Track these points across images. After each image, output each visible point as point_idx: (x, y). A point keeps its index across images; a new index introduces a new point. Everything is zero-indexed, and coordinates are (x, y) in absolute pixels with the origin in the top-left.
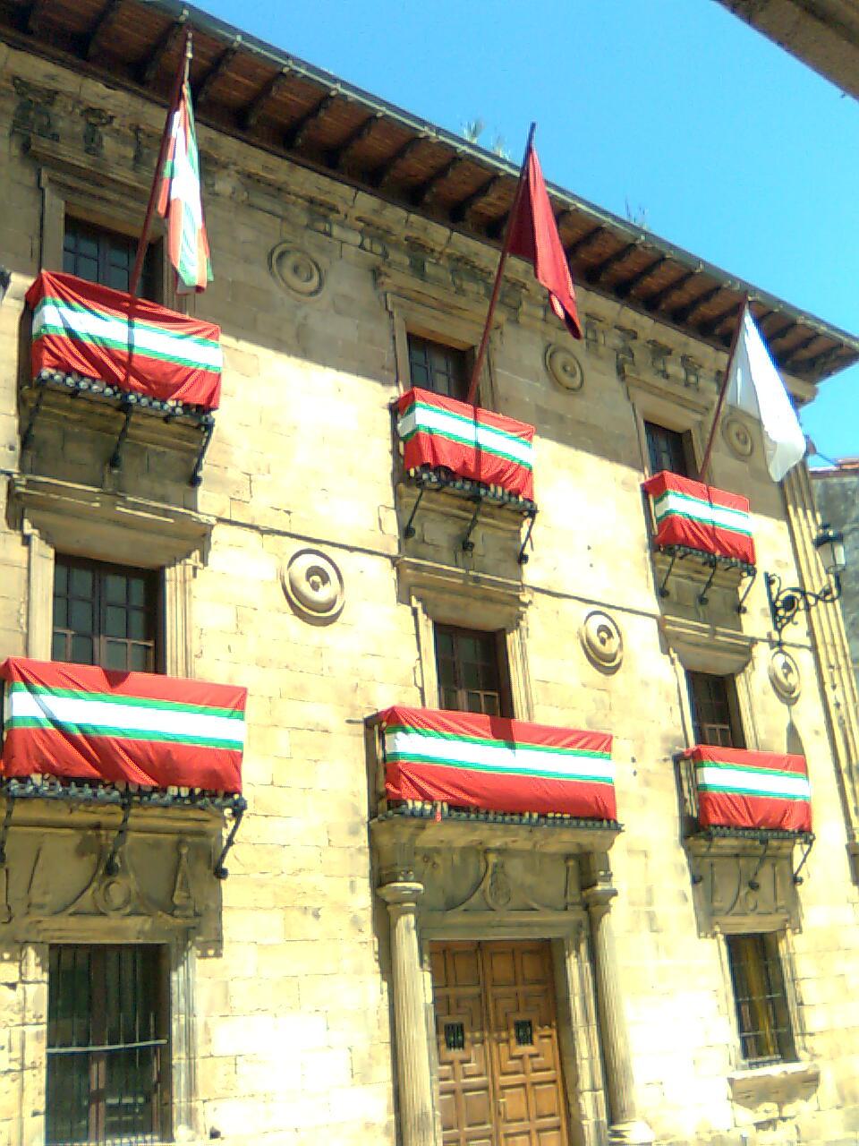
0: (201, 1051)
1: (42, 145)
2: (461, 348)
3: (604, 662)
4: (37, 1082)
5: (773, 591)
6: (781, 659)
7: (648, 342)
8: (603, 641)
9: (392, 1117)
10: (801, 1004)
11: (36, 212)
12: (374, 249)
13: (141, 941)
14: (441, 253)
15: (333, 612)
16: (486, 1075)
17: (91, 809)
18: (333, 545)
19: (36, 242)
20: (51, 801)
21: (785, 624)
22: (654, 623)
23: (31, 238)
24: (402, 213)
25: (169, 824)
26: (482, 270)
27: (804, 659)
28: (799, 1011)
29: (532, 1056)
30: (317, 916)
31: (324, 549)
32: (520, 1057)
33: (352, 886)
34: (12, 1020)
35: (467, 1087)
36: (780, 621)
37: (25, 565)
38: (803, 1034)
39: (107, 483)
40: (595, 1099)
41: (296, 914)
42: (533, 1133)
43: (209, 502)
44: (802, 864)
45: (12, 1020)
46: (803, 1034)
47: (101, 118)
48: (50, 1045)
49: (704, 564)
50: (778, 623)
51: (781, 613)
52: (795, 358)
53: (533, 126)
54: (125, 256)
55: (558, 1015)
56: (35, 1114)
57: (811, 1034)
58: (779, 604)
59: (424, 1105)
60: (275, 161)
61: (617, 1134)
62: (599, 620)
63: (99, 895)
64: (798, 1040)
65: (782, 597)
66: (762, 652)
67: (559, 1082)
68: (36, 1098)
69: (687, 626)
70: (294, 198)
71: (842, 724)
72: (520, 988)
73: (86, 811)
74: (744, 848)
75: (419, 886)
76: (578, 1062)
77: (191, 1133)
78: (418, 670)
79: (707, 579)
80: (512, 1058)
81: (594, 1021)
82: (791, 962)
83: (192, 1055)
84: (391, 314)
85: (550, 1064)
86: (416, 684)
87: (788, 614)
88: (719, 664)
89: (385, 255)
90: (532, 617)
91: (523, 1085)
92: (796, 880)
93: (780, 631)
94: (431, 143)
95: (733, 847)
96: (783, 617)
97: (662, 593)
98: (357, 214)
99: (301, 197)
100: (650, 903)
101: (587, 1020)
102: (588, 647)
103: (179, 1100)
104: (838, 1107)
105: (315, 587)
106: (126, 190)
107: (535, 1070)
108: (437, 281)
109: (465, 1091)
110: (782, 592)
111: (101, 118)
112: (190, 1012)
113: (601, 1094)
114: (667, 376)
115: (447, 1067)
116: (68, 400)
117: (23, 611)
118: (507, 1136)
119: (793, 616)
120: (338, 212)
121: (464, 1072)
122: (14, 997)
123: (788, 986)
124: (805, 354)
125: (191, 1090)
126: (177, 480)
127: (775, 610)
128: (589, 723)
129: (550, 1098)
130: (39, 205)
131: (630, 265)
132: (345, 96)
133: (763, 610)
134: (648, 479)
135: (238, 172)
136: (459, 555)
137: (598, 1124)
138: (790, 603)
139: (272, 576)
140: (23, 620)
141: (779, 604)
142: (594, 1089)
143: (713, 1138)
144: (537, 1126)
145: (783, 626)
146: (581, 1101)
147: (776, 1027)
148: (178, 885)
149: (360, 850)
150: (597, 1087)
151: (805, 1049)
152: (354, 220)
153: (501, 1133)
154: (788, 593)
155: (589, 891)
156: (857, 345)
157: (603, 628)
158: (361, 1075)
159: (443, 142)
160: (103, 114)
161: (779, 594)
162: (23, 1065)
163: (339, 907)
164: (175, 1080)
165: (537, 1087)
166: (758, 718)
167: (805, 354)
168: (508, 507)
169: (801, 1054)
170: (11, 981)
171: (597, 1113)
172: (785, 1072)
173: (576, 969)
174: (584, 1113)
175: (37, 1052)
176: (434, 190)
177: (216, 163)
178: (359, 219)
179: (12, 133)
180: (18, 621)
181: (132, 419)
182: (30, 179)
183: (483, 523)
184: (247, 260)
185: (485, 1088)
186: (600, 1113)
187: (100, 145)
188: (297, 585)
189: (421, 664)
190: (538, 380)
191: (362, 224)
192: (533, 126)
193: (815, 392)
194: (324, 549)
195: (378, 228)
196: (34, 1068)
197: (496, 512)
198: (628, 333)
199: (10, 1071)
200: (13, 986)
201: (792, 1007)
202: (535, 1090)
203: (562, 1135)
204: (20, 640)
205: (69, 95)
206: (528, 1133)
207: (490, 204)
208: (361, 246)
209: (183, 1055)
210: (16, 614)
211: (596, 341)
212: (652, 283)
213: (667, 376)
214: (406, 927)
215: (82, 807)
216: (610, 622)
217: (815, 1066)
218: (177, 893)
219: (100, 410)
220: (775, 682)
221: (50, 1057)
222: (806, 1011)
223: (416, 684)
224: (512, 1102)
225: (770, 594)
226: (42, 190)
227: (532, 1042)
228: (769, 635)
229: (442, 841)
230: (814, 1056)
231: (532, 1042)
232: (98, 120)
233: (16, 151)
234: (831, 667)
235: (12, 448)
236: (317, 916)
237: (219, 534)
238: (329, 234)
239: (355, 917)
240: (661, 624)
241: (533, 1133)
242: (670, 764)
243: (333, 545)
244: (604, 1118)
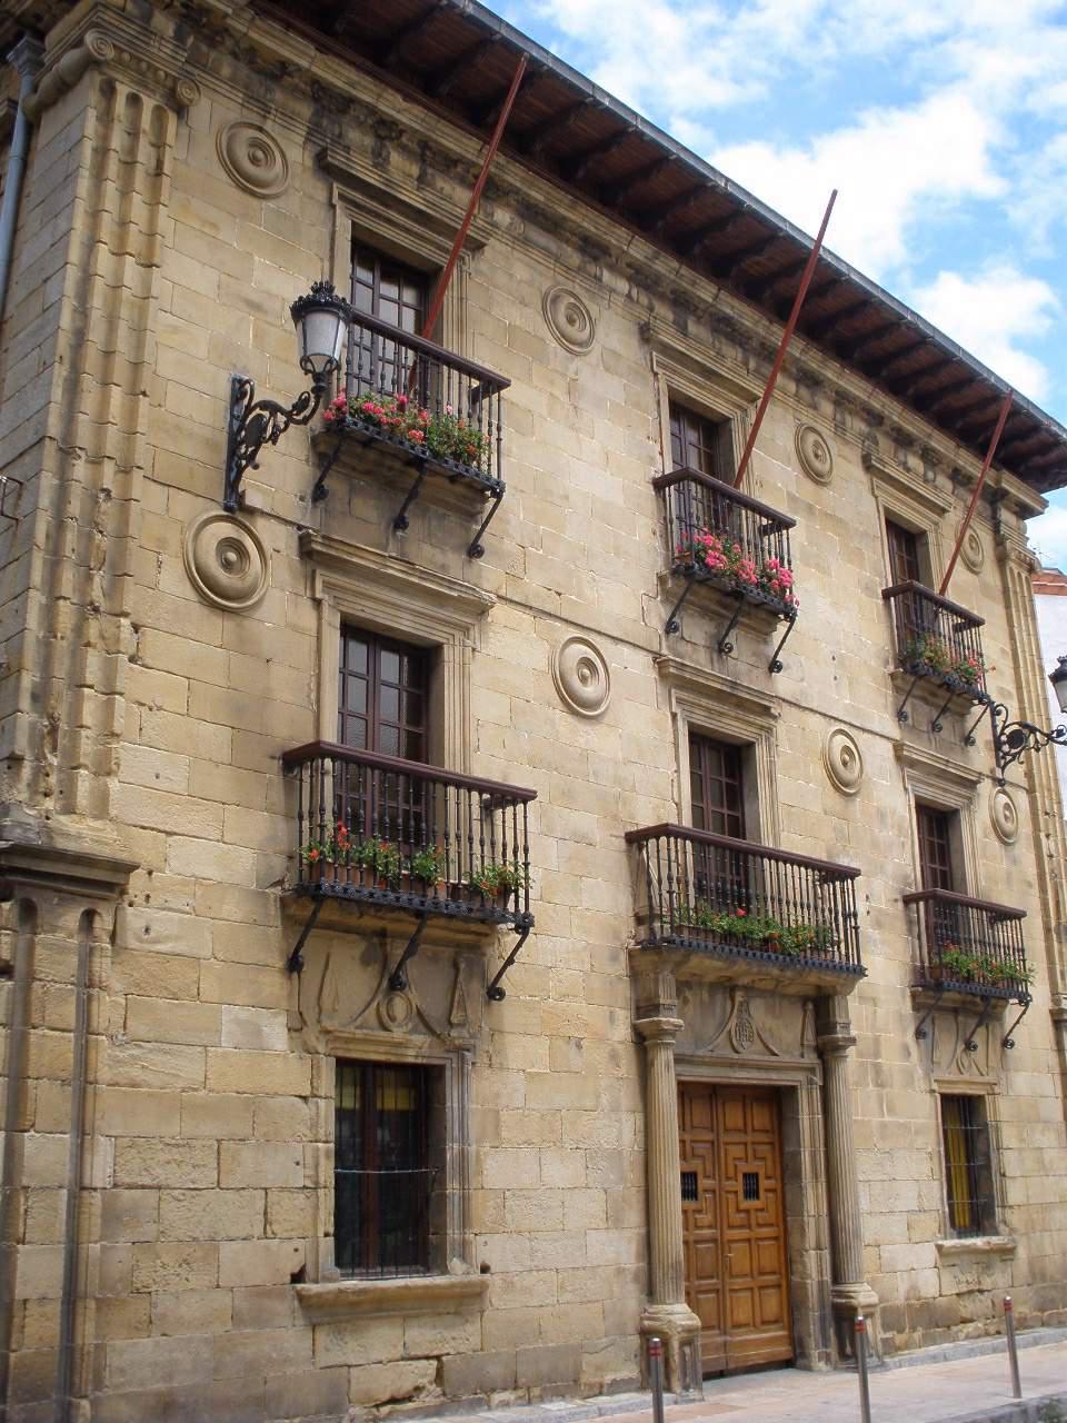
0: (474, 1183)
1: (337, 159)
2: (716, 419)
3: (842, 785)
4: (327, 1200)
5: (997, 723)
6: (1003, 799)
7: (893, 429)
8: (845, 764)
9: (643, 1264)
10: (1004, 1175)
11: (326, 231)
12: (640, 300)
13: (419, 1061)
14: (704, 311)
15: (255, 598)
16: (716, 1228)
17: (380, 914)
18: (599, 633)
19: (327, 264)
20: (346, 903)
21: (1010, 761)
22: (889, 746)
23: (322, 260)
24: (675, 264)
25: (451, 935)
26: (741, 335)
27: (1022, 799)
28: (1001, 1181)
29: (757, 1210)
30: (579, 1046)
31: (592, 638)
32: (747, 1211)
33: (612, 1016)
34: (305, 1136)
35: (699, 1238)
36: (1003, 758)
37: (314, 633)
38: (1004, 1207)
39: (391, 546)
40: (820, 1259)
41: (560, 1042)
42: (756, 1290)
43: (488, 576)
44: (1015, 1025)
45: (305, 1136)
46: (1004, 1207)
47: (391, 130)
48: (336, 1168)
49: (940, 686)
50: (1002, 760)
51: (1006, 748)
52: (1030, 464)
53: (835, 194)
54: (397, 289)
55: (788, 1170)
56: (326, 1235)
57: (1011, 1207)
58: (1004, 738)
59: (678, 1253)
60: (559, 194)
61: (840, 1294)
62: (841, 740)
63: (383, 1011)
64: (998, 1211)
65: (1007, 731)
66: (986, 787)
67: (782, 1240)
68: (327, 1222)
69: (921, 750)
70: (568, 234)
71: (1055, 877)
72: (749, 1138)
73: (375, 916)
74: (964, 1002)
75: (681, 1022)
76: (806, 1218)
77: (465, 1266)
78: (675, 784)
79: (943, 704)
80: (738, 1211)
81: (823, 1178)
82: (997, 1129)
83: (466, 1187)
84: (656, 374)
85: (773, 1220)
86: (673, 799)
87: (1013, 751)
88: (946, 798)
89: (651, 309)
90: (781, 728)
91: (749, 1240)
92: (1006, 1043)
93: (1003, 769)
94: (717, 193)
95: (954, 1001)
96: (1007, 754)
97: (901, 715)
98: (628, 260)
99: (575, 234)
100: (877, 1054)
101: (816, 1176)
102: (832, 773)
103: (453, 1233)
104: (1029, 1285)
105: (584, 679)
106: (736, 390)
107: (760, 1225)
108: (698, 340)
109: (697, 1242)
110: (1007, 726)
111: (391, 130)
112: (464, 1139)
113: (826, 1254)
114: (908, 470)
115: (743, 1215)
116: (359, 450)
117: (313, 686)
118: (732, 1290)
119: (255, 452)
120: (610, 256)
121: (696, 1223)
122: (305, 1110)
123: (993, 1155)
124: (1038, 460)
125: (465, 1222)
126: (456, 549)
127: (998, 745)
128: (829, 854)
129: (769, 1256)
130: (330, 225)
131: (889, 343)
132: (643, 134)
133: (987, 742)
134: (890, 585)
135: (517, 201)
136: (715, 656)
137: (821, 1284)
138: (1017, 739)
139: (543, 664)
140: (313, 696)
141: (1004, 738)
142: (818, 1248)
143: (922, 1305)
144: (759, 1284)
145: (1006, 764)
146: (806, 1260)
147: (971, 1198)
148: (456, 1004)
149: (619, 978)
150: (823, 1246)
151: (1005, 1222)
152: (624, 266)
153: (727, 1288)
154: (1016, 727)
155: (826, 1037)
156: (1064, 436)
157: (587, 662)
158: (613, 1220)
159: (731, 194)
160: (394, 127)
161: (1004, 728)
162: (317, 1183)
163: (601, 1039)
164: (449, 1209)
165: (761, 1243)
166: (980, 862)
167: (1038, 460)
168: (709, 583)
169: (1002, 1227)
170: (303, 1094)
171: (821, 1273)
172: (989, 1243)
173: (807, 1116)
174: (809, 1272)
175: (327, 1172)
176: (706, 242)
177: (498, 190)
178: (629, 265)
179: (307, 140)
180: (308, 696)
181: (427, 478)
182: (322, 195)
183: (743, 624)
184: (523, 303)
185: (714, 1241)
186: (824, 1272)
187: (387, 160)
188: (568, 677)
189: (679, 776)
190: (789, 465)
191: (632, 271)
192: (835, 194)
193: (1045, 504)
194: (592, 638)
195: (647, 278)
196: (325, 1187)
197: (753, 611)
198: (874, 418)
199: (305, 1187)
200: (304, 1098)
201: (996, 1178)
202: (758, 1246)
203: (781, 1293)
204: (310, 718)
205: (366, 106)
206: (751, 1289)
207: (758, 263)
208: (629, 296)
209: (456, 1185)
210: (306, 688)
211: (844, 423)
212: (904, 365)
213: (908, 470)
214: (663, 1059)
215: (372, 912)
216: (589, 650)
217: (1014, 1241)
218: (454, 1012)
219: (388, 462)
220: (995, 824)
221: (337, 1176)
222: (1009, 1183)
223: (673, 799)
224: (738, 1256)
225: (994, 727)
226: (333, 207)
227: (758, 1198)
228: (992, 771)
229: (695, 975)
230: (1012, 1231)
231: (758, 1198)
232: (387, 133)
233: (309, 162)
234: (1047, 814)
235: (302, 499)
236: (579, 1046)
237: (499, 612)
238: (600, 279)
239: (613, 1050)
240: (898, 748)
241: (756, 1290)
242: (900, 905)
243: (599, 633)
244: (828, 1277)
